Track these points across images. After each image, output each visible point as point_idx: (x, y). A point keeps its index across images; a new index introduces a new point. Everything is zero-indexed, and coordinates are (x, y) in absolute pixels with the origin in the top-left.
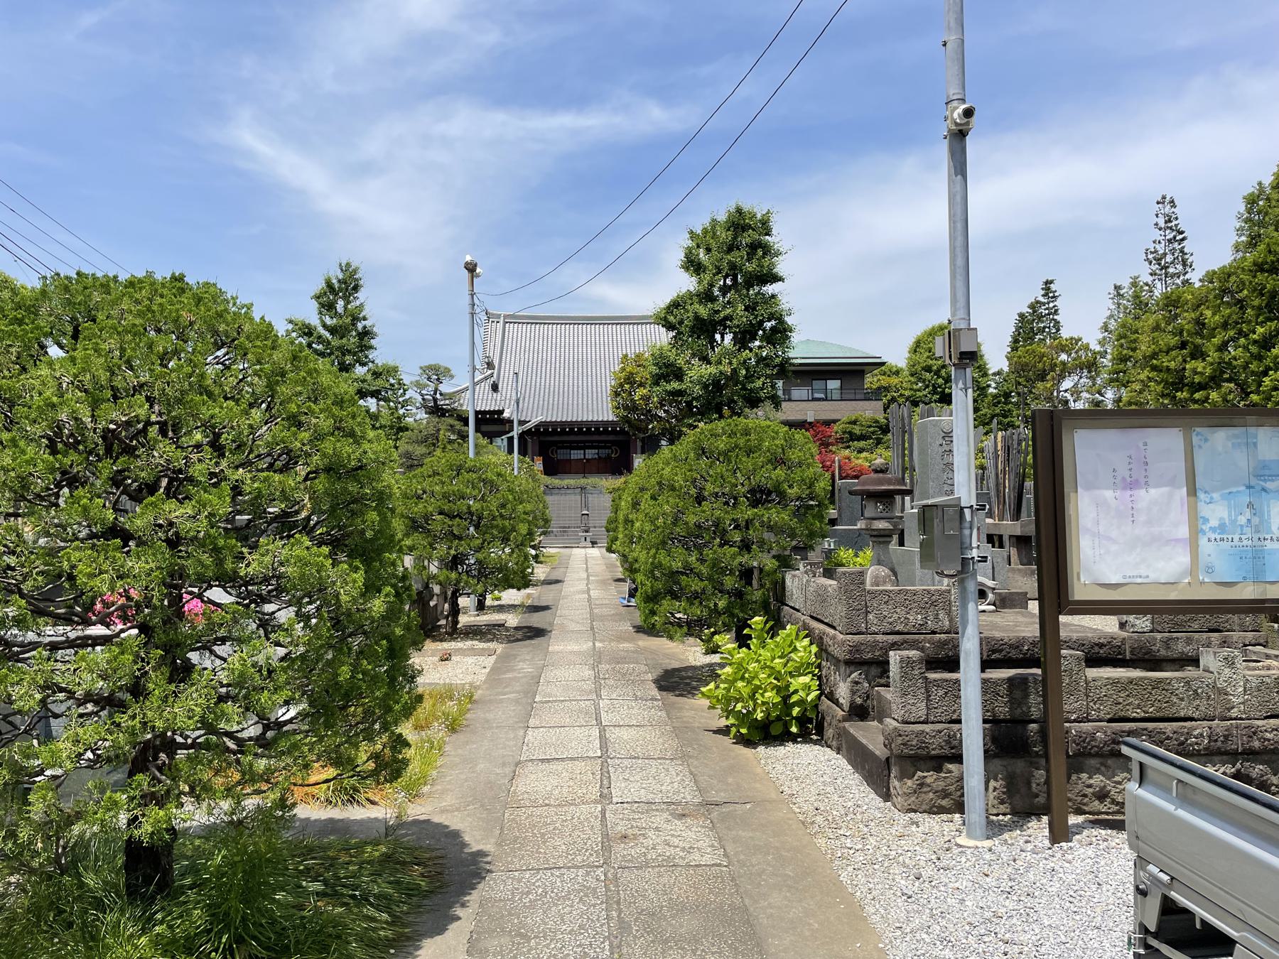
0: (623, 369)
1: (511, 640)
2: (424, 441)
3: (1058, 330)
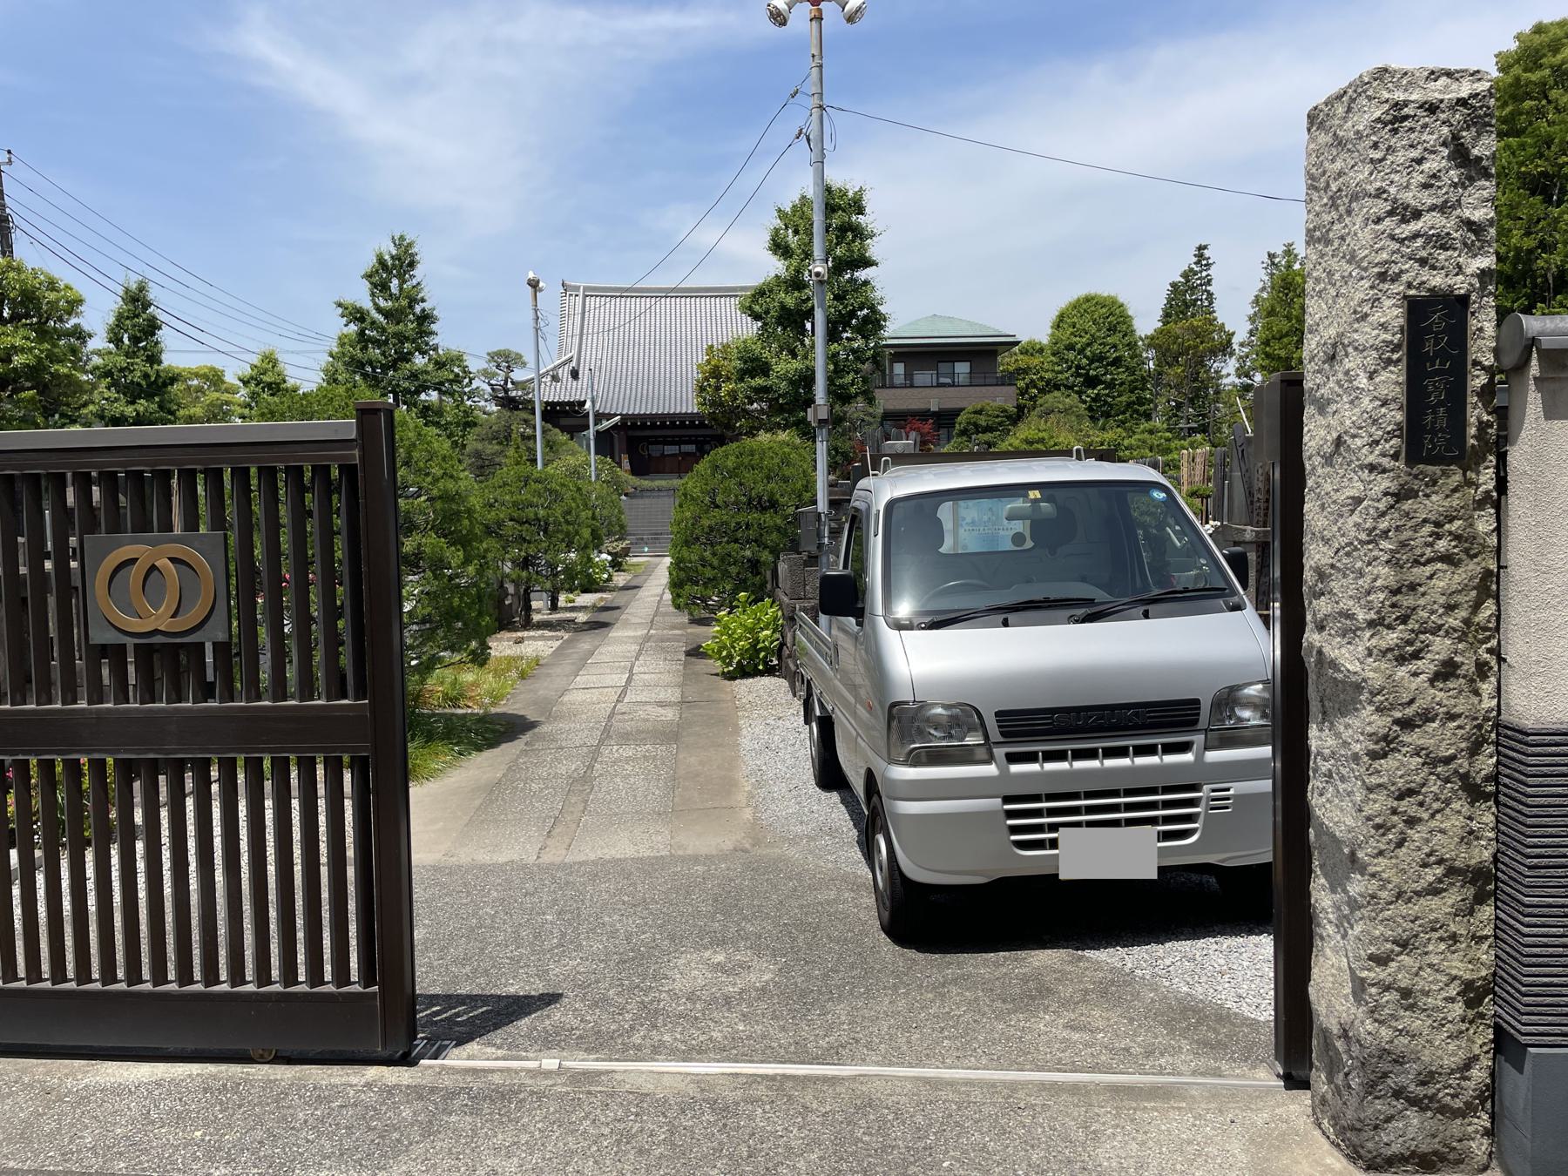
0: (708, 362)
1: (576, 630)
2: (495, 437)
3: (1211, 303)
